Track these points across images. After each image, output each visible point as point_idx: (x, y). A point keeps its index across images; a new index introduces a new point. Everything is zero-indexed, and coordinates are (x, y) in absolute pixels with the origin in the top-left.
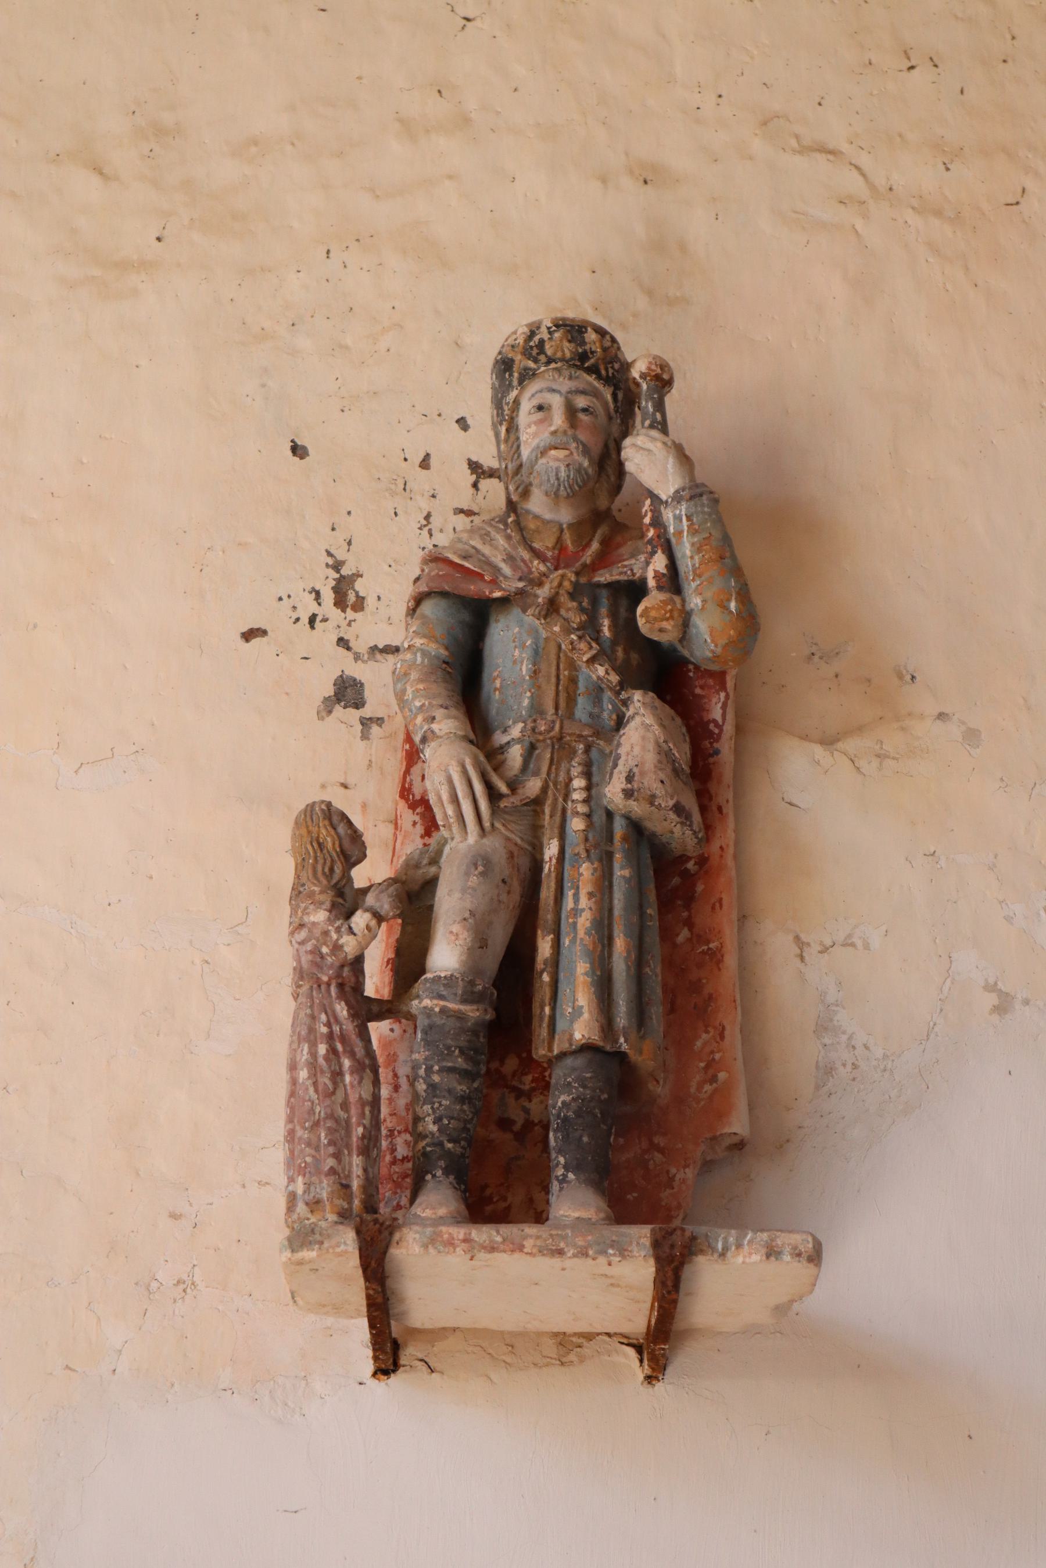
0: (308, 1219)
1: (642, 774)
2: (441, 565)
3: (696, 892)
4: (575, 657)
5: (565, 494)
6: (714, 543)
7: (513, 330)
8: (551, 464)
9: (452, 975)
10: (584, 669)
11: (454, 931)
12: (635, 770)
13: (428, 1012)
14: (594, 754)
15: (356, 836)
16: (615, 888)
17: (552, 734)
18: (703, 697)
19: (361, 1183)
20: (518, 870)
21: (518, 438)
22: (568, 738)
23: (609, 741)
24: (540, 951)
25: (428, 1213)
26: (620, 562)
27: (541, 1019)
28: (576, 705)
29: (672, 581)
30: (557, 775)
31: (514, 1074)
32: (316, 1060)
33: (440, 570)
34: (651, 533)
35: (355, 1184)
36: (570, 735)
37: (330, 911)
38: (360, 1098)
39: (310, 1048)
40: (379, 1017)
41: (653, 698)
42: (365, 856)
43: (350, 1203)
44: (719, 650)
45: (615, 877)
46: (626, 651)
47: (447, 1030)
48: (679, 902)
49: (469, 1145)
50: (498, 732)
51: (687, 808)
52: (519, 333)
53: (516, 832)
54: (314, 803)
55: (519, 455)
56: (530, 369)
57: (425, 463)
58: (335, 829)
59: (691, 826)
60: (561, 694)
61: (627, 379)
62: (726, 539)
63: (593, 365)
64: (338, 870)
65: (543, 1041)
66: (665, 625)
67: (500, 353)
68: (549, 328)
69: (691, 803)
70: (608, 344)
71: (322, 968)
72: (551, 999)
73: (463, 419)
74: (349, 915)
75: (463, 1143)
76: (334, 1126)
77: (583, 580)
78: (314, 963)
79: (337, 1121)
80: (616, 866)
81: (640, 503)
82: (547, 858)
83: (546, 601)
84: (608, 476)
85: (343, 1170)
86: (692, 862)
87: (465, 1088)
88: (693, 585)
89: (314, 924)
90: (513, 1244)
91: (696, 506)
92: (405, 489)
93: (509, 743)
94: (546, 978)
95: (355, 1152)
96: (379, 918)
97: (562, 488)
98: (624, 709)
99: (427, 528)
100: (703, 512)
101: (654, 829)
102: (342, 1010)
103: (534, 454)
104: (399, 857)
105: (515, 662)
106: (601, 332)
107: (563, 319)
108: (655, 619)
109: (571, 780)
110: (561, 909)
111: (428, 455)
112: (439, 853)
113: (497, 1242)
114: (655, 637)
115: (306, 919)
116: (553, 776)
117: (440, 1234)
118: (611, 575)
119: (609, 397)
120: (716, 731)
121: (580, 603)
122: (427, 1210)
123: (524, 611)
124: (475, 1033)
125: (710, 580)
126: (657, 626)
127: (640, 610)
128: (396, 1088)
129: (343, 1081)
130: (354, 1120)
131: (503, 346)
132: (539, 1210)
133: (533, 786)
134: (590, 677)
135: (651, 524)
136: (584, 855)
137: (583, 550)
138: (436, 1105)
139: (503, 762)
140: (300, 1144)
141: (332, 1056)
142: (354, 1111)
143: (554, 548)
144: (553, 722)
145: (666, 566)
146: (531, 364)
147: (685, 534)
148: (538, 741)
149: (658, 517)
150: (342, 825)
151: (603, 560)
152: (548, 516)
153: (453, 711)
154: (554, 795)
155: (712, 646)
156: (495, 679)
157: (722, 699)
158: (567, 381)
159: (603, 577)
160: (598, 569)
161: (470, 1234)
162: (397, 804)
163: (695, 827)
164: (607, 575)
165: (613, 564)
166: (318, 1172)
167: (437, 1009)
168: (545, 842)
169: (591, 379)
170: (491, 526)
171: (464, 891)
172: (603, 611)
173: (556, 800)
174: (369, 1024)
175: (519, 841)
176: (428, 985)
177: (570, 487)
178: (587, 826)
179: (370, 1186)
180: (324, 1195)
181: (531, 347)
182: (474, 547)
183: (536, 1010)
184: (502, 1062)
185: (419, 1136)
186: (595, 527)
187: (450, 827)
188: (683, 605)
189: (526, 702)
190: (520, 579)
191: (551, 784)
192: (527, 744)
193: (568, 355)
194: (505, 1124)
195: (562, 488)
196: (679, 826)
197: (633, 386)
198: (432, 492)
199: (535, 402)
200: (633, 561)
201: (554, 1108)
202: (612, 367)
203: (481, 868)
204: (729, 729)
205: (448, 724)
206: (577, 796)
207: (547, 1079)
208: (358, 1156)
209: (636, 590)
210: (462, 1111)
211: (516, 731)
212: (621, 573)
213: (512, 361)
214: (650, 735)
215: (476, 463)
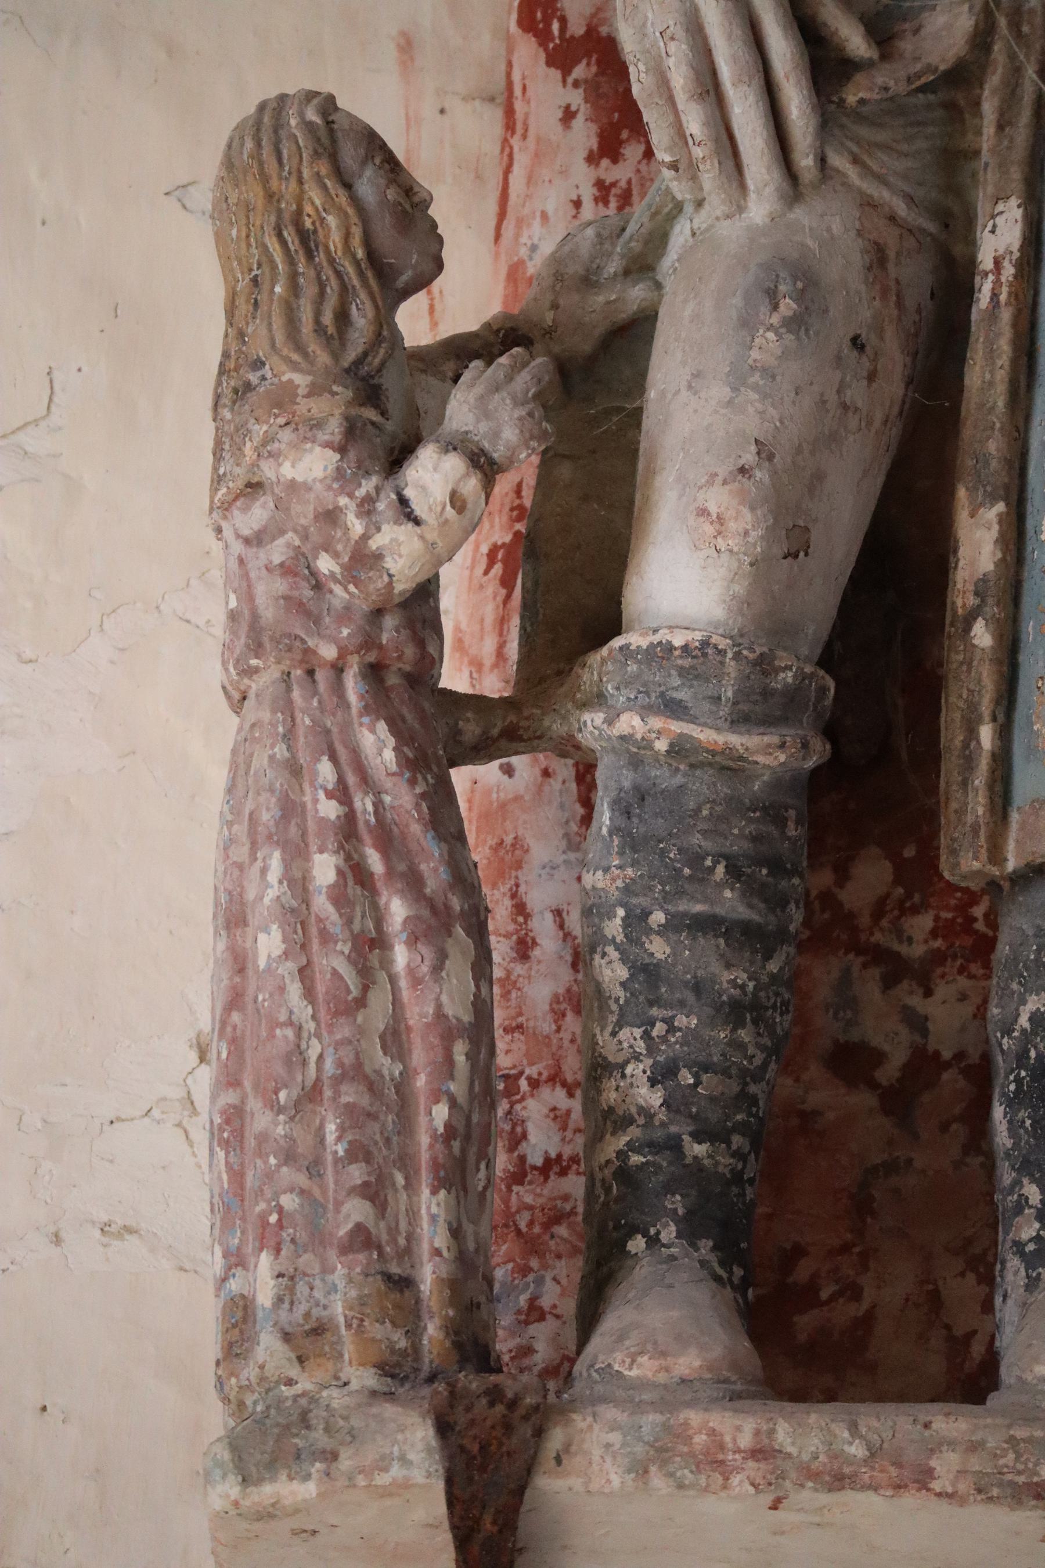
0: (290, 1382)
9: (705, 643)
11: (713, 509)
13: (634, 752)
15: (411, 208)
19: (444, 1272)
20: (899, 304)
24: (962, 552)
25: (645, 1368)
27: (969, 762)
31: (879, 911)
32: (307, 902)
35: (428, 1276)
37: (342, 450)
38: (440, 1014)
39: (287, 865)
40: (479, 752)
42: (439, 266)
43: (414, 1333)
47: (692, 805)
49: (756, 1144)
53: (887, 180)
54: (283, 98)
58: (348, 186)
64: (362, 320)
65: (975, 830)
71: (317, 621)
72: (997, 702)
74: (397, 457)
75: (737, 1140)
76: (365, 1101)
78: (294, 605)
79: (373, 1086)
82: (985, 260)
85: (393, 1231)
87: (742, 977)
89: (293, 486)
90: (898, 1465)
94: (982, 635)
95: (425, 1178)
96: (485, 465)
102: (378, 746)
104: (520, 223)
110: (1028, 418)
112: (658, 240)
113: (850, 1460)
115: (268, 471)
117: (682, 1434)
122: (643, 1359)
124: (773, 813)
128: (524, 948)
129: (387, 963)
130: (421, 1081)
132: (959, 1332)
138: (659, 1029)
140: (261, 1153)
141: (354, 890)
142: (419, 1056)
150: (369, 172)
154: (1012, 57)
161: (772, 1432)
162: (510, 51)
166: (318, 1239)
167: (661, 745)
168: (982, 207)
171: (737, 380)
173: (1017, 71)
174: (453, 772)
175: (901, 208)
176: (632, 667)
179: (468, 1270)
180: (338, 1310)
183: (951, 736)
184: (842, 874)
185: (606, 1120)
191: (1002, 22)
194: (852, 1061)
201: (1008, 1032)
203: (788, 306)
207: (980, 926)
208: (434, 1192)
210: (739, 1046)
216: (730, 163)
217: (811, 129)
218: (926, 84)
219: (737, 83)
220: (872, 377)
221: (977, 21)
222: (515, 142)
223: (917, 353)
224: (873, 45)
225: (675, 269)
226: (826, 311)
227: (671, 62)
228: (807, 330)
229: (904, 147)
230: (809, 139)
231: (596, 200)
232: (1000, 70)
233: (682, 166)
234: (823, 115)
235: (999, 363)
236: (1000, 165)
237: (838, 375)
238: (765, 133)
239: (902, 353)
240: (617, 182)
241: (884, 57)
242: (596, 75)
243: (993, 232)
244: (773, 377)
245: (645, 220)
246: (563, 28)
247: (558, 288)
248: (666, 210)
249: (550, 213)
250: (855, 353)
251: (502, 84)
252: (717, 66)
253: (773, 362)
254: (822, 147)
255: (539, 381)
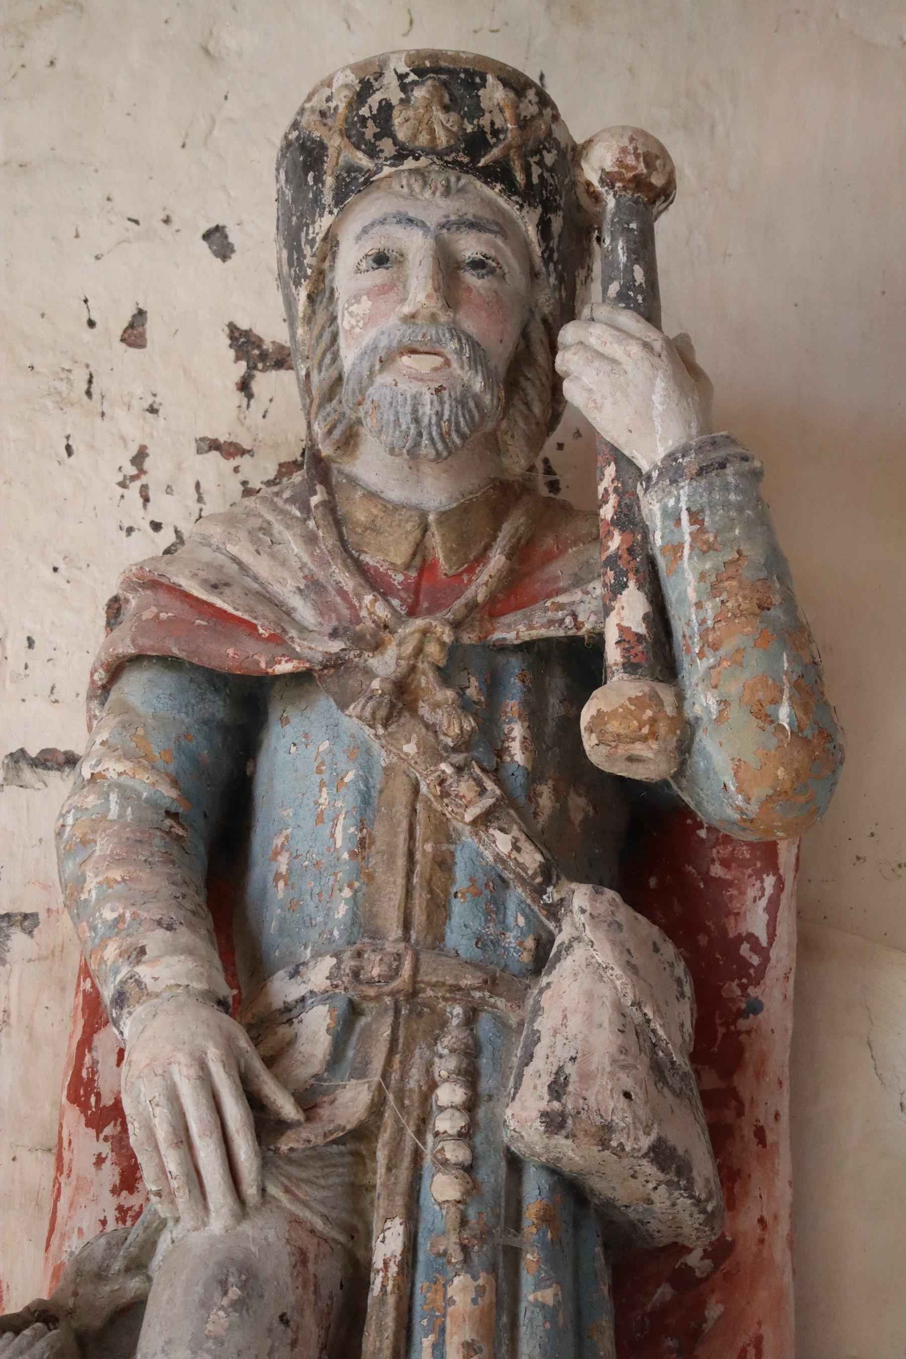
1: (586, 1077)
2: (164, 598)
3: (705, 1320)
4: (447, 811)
5: (432, 453)
6: (747, 574)
7: (325, 75)
8: (402, 386)
10: (468, 838)
12: (570, 1069)
14: (485, 1026)
16: (524, 1331)
17: (394, 984)
18: (729, 884)
20: (316, 1292)
21: (333, 319)
22: (430, 993)
23: (518, 999)
26: (549, 596)
28: (448, 916)
29: (659, 652)
30: (403, 1077)
33: (162, 608)
34: (615, 542)
36: (434, 986)
41: (612, 902)
44: (753, 809)
45: (523, 1305)
46: (558, 795)
48: (670, 1343)
50: (281, 973)
51: (680, 1151)
53: (311, 1205)
55: (336, 357)
56: (359, 170)
57: (134, 334)
59: (689, 1188)
60: (416, 894)
61: (574, 184)
62: (776, 563)
63: (496, 162)
66: (639, 749)
67: (295, 125)
68: (401, 77)
69: (691, 1138)
70: (529, 108)
73: (218, 229)
77: (469, 638)
80: (527, 1280)
81: (592, 477)
82: (378, 1263)
83: (388, 686)
84: (527, 404)
86: (698, 1253)
88: (702, 666)
91: (710, 490)
92: (89, 393)
93: (303, 999)
97: (425, 441)
98: (551, 926)
99: (138, 484)
100: (726, 504)
101: (609, 1194)
103: (366, 365)
104: (63, 1236)
105: (320, 819)
106: (517, 84)
107: (434, 56)
109: (433, 1086)
112: (149, 1246)
114: (621, 770)
116: (395, 1077)
118: (531, 627)
119: (532, 232)
120: (755, 960)
121: (461, 691)
123: (343, 706)
125: (737, 659)
126: (622, 750)
127: (587, 714)
131: (302, 111)
133: (352, 1101)
134: (480, 855)
135: (615, 523)
136: (456, 1257)
137: (471, 570)
139: (292, 1042)
143: (408, 567)
144: (399, 957)
145: (646, 618)
146: (364, 161)
147: (686, 551)
148: (366, 998)
149: (629, 507)
151: (512, 592)
152: (395, 494)
153: (185, 936)
154: (397, 1121)
155: (739, 800)
156: (277, 853)
157: (769, 890)
159: (513, 630)
160: (503, 614)
162: (62, 1116)
163: (700, 1190)
164: (522, 628)
168: (376, 1225)
169: (493, 193)
170: (275, 508)
172: (512, 705)
173: (400, 1131)
178: (467, 1193)
181: (363, 120)
182: (234, 559)
186: (498, 516)
187: (172, 1194)
188: (680, 708)
189: (342, 911)
190: (334, 634)
192: (341, 1004)
193: (443, 140)
195: (425, 441)
196: (663, 1188)
197: (585, 201)
199: (371, 245)
200: (578, 595)
202: (541, 163)
203: (234, 1292)
204: (782, 955)
205: (174, 967)
206: (447, 1123)
209: (580, 663)
211: (318, 975)
212: (551, 623)
213: (322, 147)
214: (605, 990)
215: (247, 333)
216: (197, 1191)
217: (254, 1168)
218: (337, 1138)
219: (202, 1135)
220: (294, 1344)
221: (373, 1096)
222: (62, 1179)
223: (329, 1328)
224: (300, 1111)
225: (160, 1267)
226: (261, 1296)
227: (156, 1121)
228: (247, 1309)
229: (322, 1182)
230: (253, 1175)
231: (117, 1219)
232: (389, 1131)
233: (164, 1194)
234: (263, 1158)
235: (386, 1335)
236: (389, 1195)
237: (269, 1342)
238: (221, 1171)
239: (318, 1327)
240: (132, 1207)
241: (308, 1119)
242: (120, 1132)
243: (383, 1242)
244: (222, 1343)
245: (140, 1232)
246: (98, 1101)
247: (78, 1280)
248: (155, 1225)
249: (84, 1230)
250: (282, 1327)
251: (56, 1141)
252: (189, 1124)
253: (222, 1332)
254: (263, 1181)
255: (52, 1347)
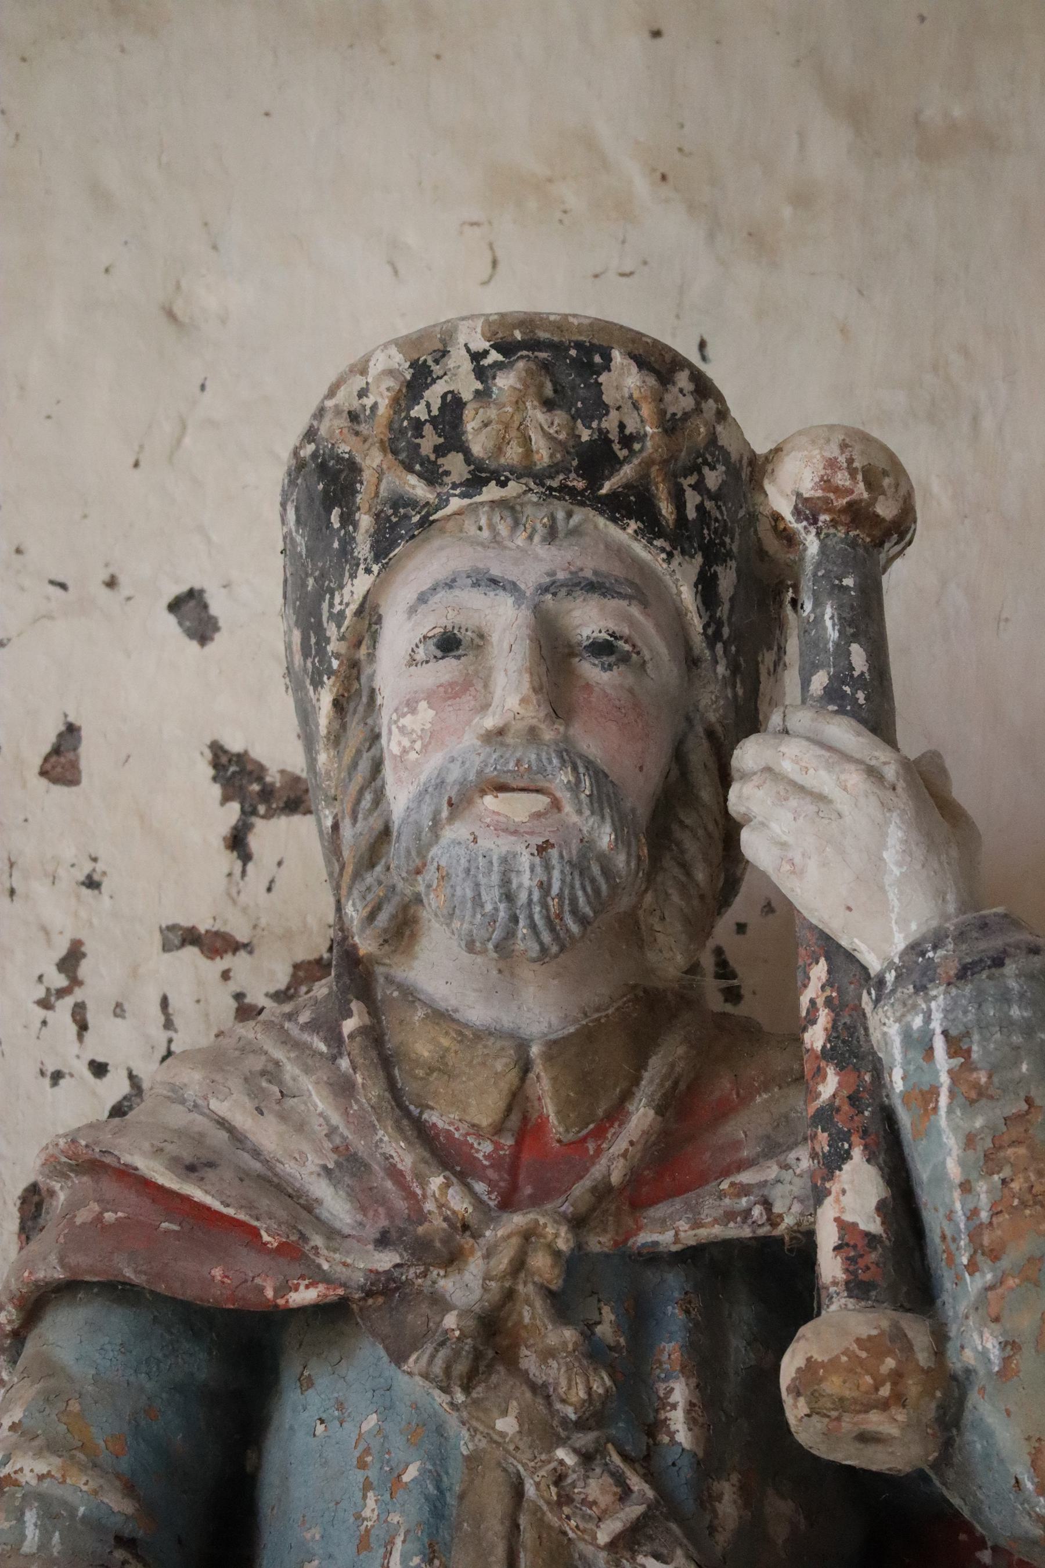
2: (110, 1188)
5: (534, 949)
7: (355, 356)
8: (486, 843)
26: (726, 1173)
29: (904, 1262)
34: (829, 1086)
46: (747, 1495)
52: (374, 370)
56: (413, 503)
61: (753, 518)
63: (628, 486)
66: (875, 1421)
67: (310, 435)
68: (477, 357)
70: (680, 401)
77: (598, 1242)
84: (685, 867)
88: (974, 1284)
97: (522, 929)
99: (69, 1002)
100: (1006, 1024)
103: (427, 810)
105: (364, 1543)
106: (659, 363)
107: (528, 322)
108: (841, 1404)
111: (71, 731)
118: (697, 1225)
119: (687, 596)
121: (588, 1330)
123: (398, 1358)
126: (848, 1424)
127: (790, 1365)
135: (827, 1055)
137: (599, 1133)
143: (498, 1129)
145: (881, 1208)
146: (418, 488)
147: (944, 1100)
149: (851, 1029)
151: (667, 1168)
152: (477, 1013)
158: (540, 549)
160: (653, 1202)
164: (683, 1225)
165: (702, 1179)
169: (625, 535)
172: (670, 1350)
177: (552, 928)
181: (418, 425)
182: (222, 1123)
188: (939, 1352)
190: (383, 1241)
193: (543, 454)
195: (522, 929)
197: (772, 545)
198: (87, 867)
200: (771, 1171)
202: (699, 487)
209: (776, 1279)
212: (730, 1216)
213: (353, 468)
215: (241, 758)
